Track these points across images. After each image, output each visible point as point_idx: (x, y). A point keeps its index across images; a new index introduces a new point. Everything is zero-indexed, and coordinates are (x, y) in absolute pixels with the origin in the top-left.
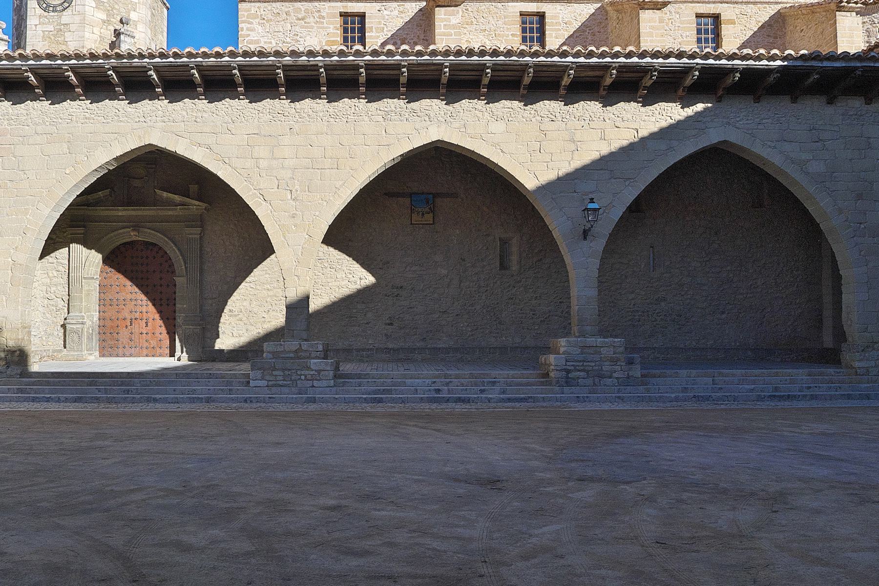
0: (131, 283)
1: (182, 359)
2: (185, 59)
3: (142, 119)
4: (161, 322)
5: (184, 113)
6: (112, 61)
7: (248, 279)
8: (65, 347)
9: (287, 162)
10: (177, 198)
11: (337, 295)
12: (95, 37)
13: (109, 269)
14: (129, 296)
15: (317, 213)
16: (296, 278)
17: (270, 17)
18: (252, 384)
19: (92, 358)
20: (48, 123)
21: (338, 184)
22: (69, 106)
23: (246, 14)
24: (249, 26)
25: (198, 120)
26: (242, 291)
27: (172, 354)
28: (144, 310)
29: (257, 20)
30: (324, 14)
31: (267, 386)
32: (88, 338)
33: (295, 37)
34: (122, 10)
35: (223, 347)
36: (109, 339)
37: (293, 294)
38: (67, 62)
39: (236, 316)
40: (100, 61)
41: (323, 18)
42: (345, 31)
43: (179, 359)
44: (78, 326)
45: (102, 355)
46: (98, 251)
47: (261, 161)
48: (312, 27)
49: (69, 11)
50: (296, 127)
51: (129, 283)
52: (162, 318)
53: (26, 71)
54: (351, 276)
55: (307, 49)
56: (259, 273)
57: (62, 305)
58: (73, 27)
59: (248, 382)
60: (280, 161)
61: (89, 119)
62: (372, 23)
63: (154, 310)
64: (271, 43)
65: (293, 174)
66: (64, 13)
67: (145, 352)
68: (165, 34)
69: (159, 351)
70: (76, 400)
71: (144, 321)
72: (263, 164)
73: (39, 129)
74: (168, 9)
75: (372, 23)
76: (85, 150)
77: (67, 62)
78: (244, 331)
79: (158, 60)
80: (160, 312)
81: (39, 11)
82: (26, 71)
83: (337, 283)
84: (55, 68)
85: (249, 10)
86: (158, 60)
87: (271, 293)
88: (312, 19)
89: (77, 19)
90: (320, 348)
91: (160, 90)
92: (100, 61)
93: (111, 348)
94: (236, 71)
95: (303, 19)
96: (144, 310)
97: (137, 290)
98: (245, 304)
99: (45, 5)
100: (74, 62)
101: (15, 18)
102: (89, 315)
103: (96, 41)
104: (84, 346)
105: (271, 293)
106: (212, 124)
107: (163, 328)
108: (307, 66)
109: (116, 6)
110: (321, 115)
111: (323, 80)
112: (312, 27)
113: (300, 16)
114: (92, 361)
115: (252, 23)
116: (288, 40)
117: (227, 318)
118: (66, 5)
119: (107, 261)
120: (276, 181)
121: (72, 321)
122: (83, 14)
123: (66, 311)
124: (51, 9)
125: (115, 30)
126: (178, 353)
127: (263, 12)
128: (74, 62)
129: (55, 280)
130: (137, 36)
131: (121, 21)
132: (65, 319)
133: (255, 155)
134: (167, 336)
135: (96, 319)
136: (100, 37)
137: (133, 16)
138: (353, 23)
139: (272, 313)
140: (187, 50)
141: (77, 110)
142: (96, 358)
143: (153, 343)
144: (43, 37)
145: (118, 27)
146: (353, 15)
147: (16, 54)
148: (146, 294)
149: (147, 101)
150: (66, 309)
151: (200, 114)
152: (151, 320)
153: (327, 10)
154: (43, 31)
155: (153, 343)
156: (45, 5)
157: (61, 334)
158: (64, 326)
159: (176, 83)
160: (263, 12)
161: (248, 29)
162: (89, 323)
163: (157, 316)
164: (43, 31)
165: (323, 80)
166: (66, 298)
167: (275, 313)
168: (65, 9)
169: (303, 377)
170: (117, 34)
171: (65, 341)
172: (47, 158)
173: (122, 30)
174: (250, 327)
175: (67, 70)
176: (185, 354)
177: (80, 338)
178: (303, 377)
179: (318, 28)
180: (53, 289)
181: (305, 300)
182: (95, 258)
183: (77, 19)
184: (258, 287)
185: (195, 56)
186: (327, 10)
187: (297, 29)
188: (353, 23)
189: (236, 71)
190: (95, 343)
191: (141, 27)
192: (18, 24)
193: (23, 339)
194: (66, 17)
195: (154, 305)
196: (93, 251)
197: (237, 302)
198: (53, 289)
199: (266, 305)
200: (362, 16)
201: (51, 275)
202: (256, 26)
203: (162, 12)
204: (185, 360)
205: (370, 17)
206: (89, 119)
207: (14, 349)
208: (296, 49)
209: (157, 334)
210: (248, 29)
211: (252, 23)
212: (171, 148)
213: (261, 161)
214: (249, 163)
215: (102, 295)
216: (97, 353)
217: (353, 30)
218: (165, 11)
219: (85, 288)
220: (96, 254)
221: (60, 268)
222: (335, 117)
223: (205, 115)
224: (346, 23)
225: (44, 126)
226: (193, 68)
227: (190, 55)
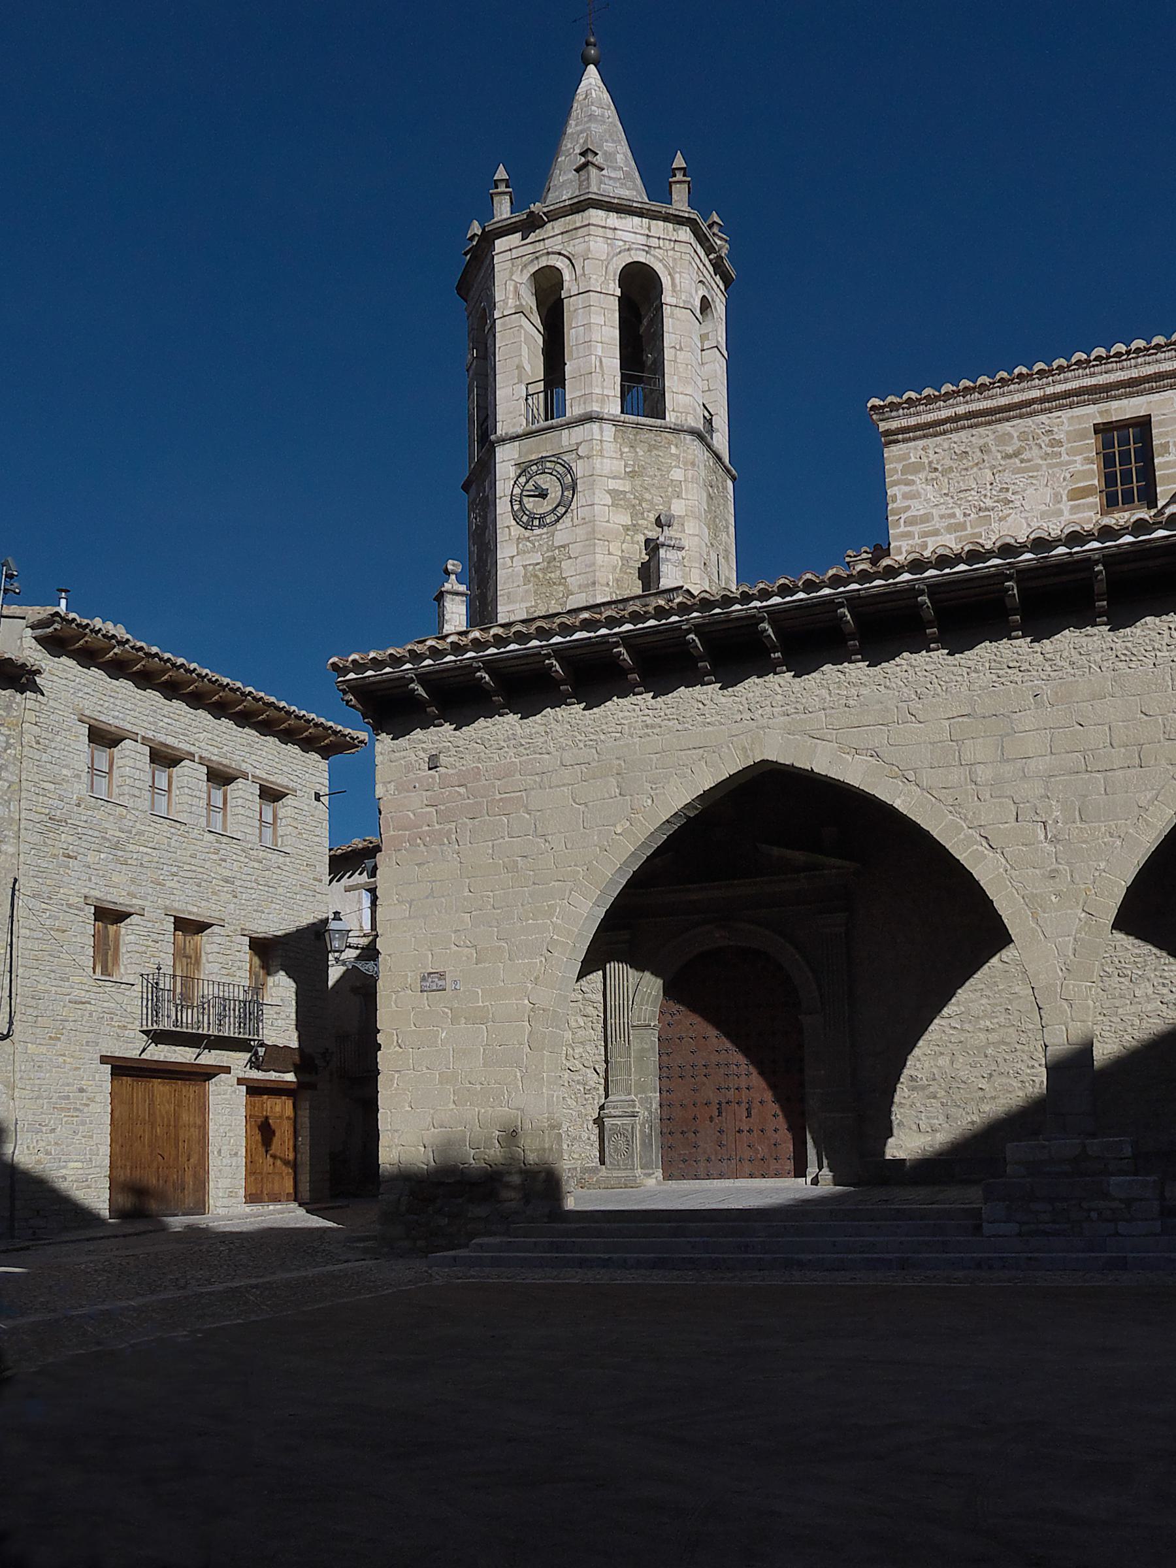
0: (716, 1032)
1: (816, 1183)
2: (827, 591)
3: (747, 715)
4: (776, 1108)
5: (824, 692)
6: (695, 614)
7: (945, 1011)
8: (602, 1162)
9: (1032, 764)
10: (799, 857)
11: (1137, 1035)
12: (616, 560)
13: (676, 1007)
14: (714, 1058)
15: (1102, 865)
16: (1065, 1005)
17: (948, 462)
18: (987, 1228)
19: (651, 1182)
20: (581, 745)
21: (1144, 798)
22: (619, 710)
23: (899, 467)
24: (907, 489)
25: (851, 702)
26: (935, 1036)
27: (800, 1172)
28: (743, 1085)
29: (922, 475)
30: (1061, 436)
31: (1019, 1235)
32: (643, 1144)
33: (1002, 495)
34: (657, 500)
35: (901, 1155)
36: (681, 1148)
37: (1061, 1040)
38: (616, 630)
39: (923, 1088)
40: (674, 618)
41: (1060, 443)
42: (1108, 461)
43: (815, 1181)
44: (627, 1121)
45: (668, 1177)
46: (656, 973)
47: (980, 769)
48: (1037, 468)
49: (566, 522)
50: (1048, 691)
51: (712, 1032)
52: (778, 1099)
53: (548, 656)
54: (1165, 991)
55: (1066, 531)
56: (969, 999)
57: (595, 1081)
58: (574, 550)
59: (978, 1229)
60: (1019, 764)
61: (652, 727)
62: (1166, 434)
63: (763, 1085)
64: (953, 515)
65: (1047, 788)
66: (559, 526)
67: (747, 1168)
68: (732, 530)
69: (774, 1166)
70: (657, 1264)
71: (744, 1106)
72: (984, 774)
73: (568, 757)
74: (734, 479)
75: (1166, 434)
76: (647, 786)
77: (616, 630)
78: (942, 1118)
79: (776, 600)
80: (773, 1086)
81: (517, 531)
82: (548, 656)
83: (1133, 1009)
84: (597, 643)
85: (906, 457)
86: (776, 600)
87: (994, 1037)
88: (1035, 450)
89: (581, 532)
90: (1128, 1151)
91: (778, 655)
92: (674, 618)
93: (684, 1161)
94: (924, 598)
95: (1016, 454)
96: (743, 1085)
97: (728, 1045)
98: (940, 1062)
99: (525, 518)
100: (628, 627)
101: (475, 549)
102: (641, 1100)
103: (615, 568)
104: (637, 1161)
105: (994, 1037)
106: (878, 707)
107: (781, 1118)
108: (1069, 563)
109: (647, 496)
110: (1098, 657)
111: (1101, 587)
112: (1037, 468)
113: (1010, 450)
114: (653, 1189)
115: (913, 482)
116: (989, 503)
117: (906, 1093)
118: (561, 510)
119: (670, 991)
120: (1013, 808)
121: (613, 1112)
122: (590, 522)
123: (602, 1092)
124: (536, 522)
125: (647, 541)
126: (812, 1170)
127: (932, 457)
128: (628, 627)
129: (581, 1032)
130: (685, 543)
131: (658, 523)
132: (602, 1108)
133: (968, 757)
134: (789, 1136)
135: (656, 1105)
136: (622, 558)
137: (678, 508)
138: (1124, 441)
139: (998, 1081)
140: (831, 573)
141: (630, 712)
142: (659, 1183)
143: (762, 1150)
144: (525, 576)
145: (651, 535)
146: (1122, 426)
147: (532, 630)
148: (746, 1051)
149: (754, 679)
150: (602, 1088)
151: (854, 691)
152: (756, 1104)
153: (1066, 427)
154: (525, 567)
155: (762, 1150)
156: (525, 518)
157: (595, 1138)
158: (599, 1122)
159: (810, 639)
160: (932, 457)
161: (906, 496)
162: (643, 1114)
163: (768, 1096)
164: (525, 567)
165: (1101, 587)
166: (601, 1068)
167: (1004, 1080)
168: (559, 518)
169: (1094, 1215)
170: (653, 547)
171: (602, 1150)
172: (582, 808)
173: (662, 539)
174: (953, 1111)
175: (617, 645)
176: (825, 1171)
177: (629, 1143)
178: (1094, 1215)
179: (1050, 466)
180: (579, 1050)
181: (1085, 1051)
182: (651, 985)
183: (581, 532)
184: (967, 1026)
185: (846, 581)
186: (1066, 427)
187: (1007, 477)
188: (1124, 441)
189: (924, 598)
190: (656, 1154)
191: (691, 527)
192: (480, 558)
193: (551, 1149)
194: (563, 533)
195: (761, 1073)
196: (647, 974)
197: (922, 1061)
198: (579, 1050)
199: (984, 1062)
200: (1144, 424)
201: (573, 1024)
202: (920, 486)
203: (725, 488)
204: (827, 1186)
205: (1161, 423)
206: (652, 727)
207: (536, 1168)
208: (1044, 535)
209: (770, 1132)
210: (906, 496)
211: (913, 482)
212: (803, 764)
213: (980, 769)
214: (956, 776)
215: (665, 1057)
216: (659, 1173)
217: (1125, 457)
218: (730, 484)
219: (635, 1045)
220: (653, 978)
221: (590, 1010)
222: (1129, 656)
223: (864, 691)
224: (1107, 444)
225: (575, 751)
226: (841, 605)
227: (836, 581)
